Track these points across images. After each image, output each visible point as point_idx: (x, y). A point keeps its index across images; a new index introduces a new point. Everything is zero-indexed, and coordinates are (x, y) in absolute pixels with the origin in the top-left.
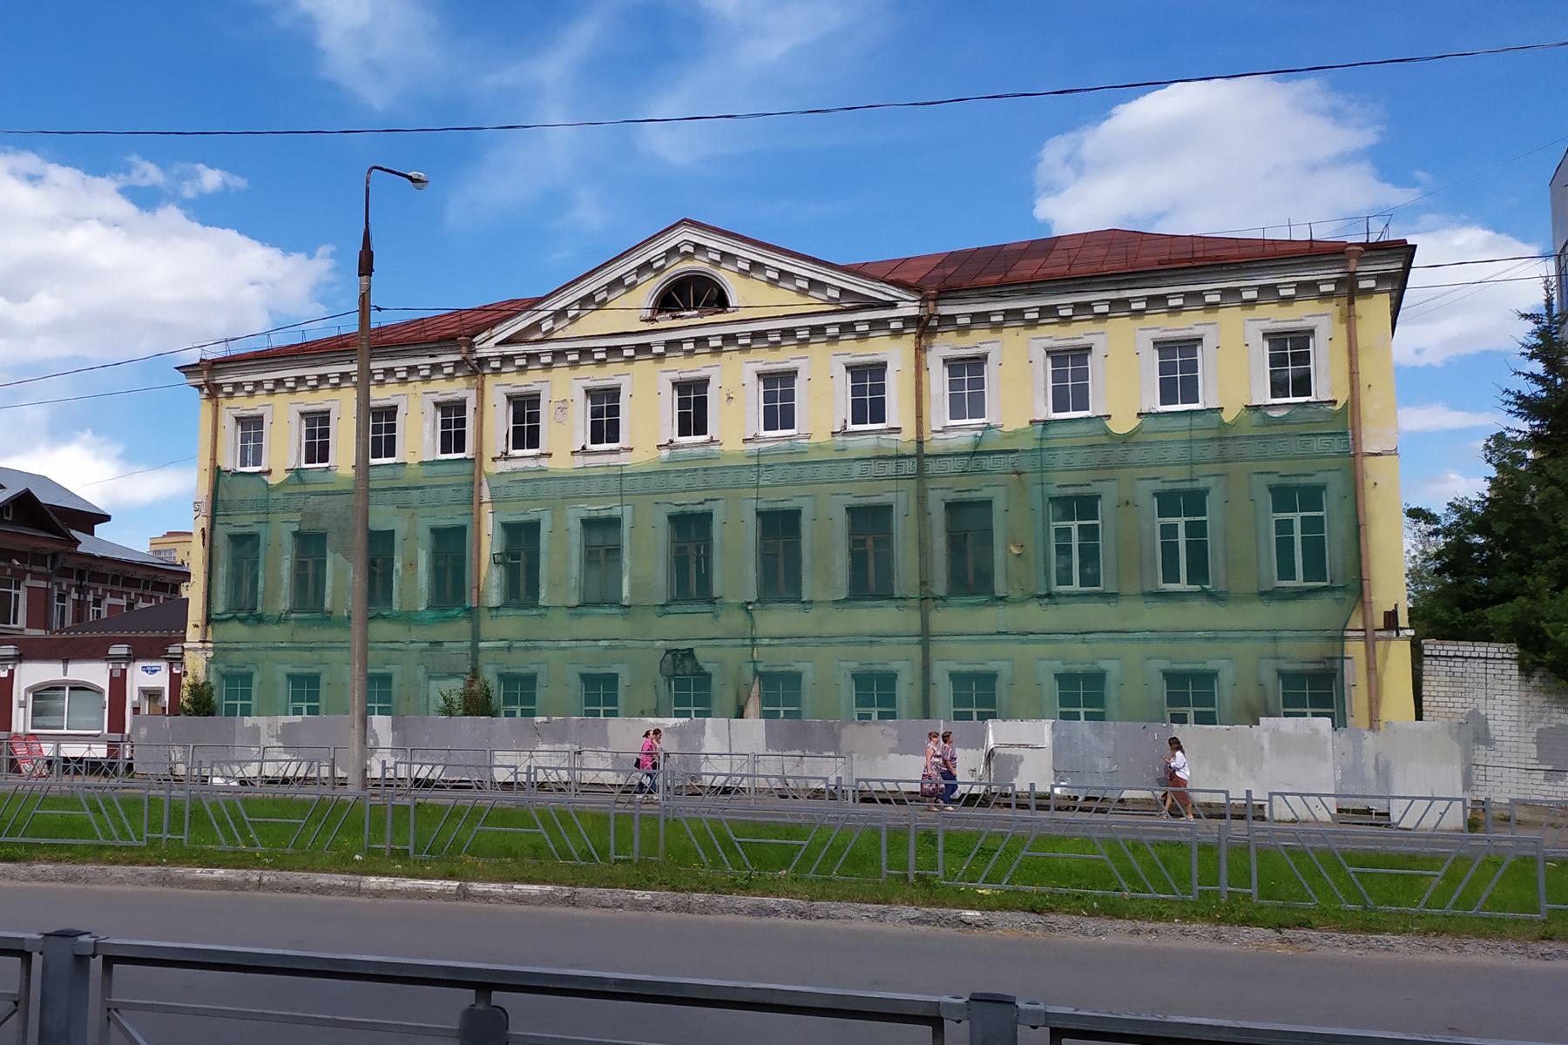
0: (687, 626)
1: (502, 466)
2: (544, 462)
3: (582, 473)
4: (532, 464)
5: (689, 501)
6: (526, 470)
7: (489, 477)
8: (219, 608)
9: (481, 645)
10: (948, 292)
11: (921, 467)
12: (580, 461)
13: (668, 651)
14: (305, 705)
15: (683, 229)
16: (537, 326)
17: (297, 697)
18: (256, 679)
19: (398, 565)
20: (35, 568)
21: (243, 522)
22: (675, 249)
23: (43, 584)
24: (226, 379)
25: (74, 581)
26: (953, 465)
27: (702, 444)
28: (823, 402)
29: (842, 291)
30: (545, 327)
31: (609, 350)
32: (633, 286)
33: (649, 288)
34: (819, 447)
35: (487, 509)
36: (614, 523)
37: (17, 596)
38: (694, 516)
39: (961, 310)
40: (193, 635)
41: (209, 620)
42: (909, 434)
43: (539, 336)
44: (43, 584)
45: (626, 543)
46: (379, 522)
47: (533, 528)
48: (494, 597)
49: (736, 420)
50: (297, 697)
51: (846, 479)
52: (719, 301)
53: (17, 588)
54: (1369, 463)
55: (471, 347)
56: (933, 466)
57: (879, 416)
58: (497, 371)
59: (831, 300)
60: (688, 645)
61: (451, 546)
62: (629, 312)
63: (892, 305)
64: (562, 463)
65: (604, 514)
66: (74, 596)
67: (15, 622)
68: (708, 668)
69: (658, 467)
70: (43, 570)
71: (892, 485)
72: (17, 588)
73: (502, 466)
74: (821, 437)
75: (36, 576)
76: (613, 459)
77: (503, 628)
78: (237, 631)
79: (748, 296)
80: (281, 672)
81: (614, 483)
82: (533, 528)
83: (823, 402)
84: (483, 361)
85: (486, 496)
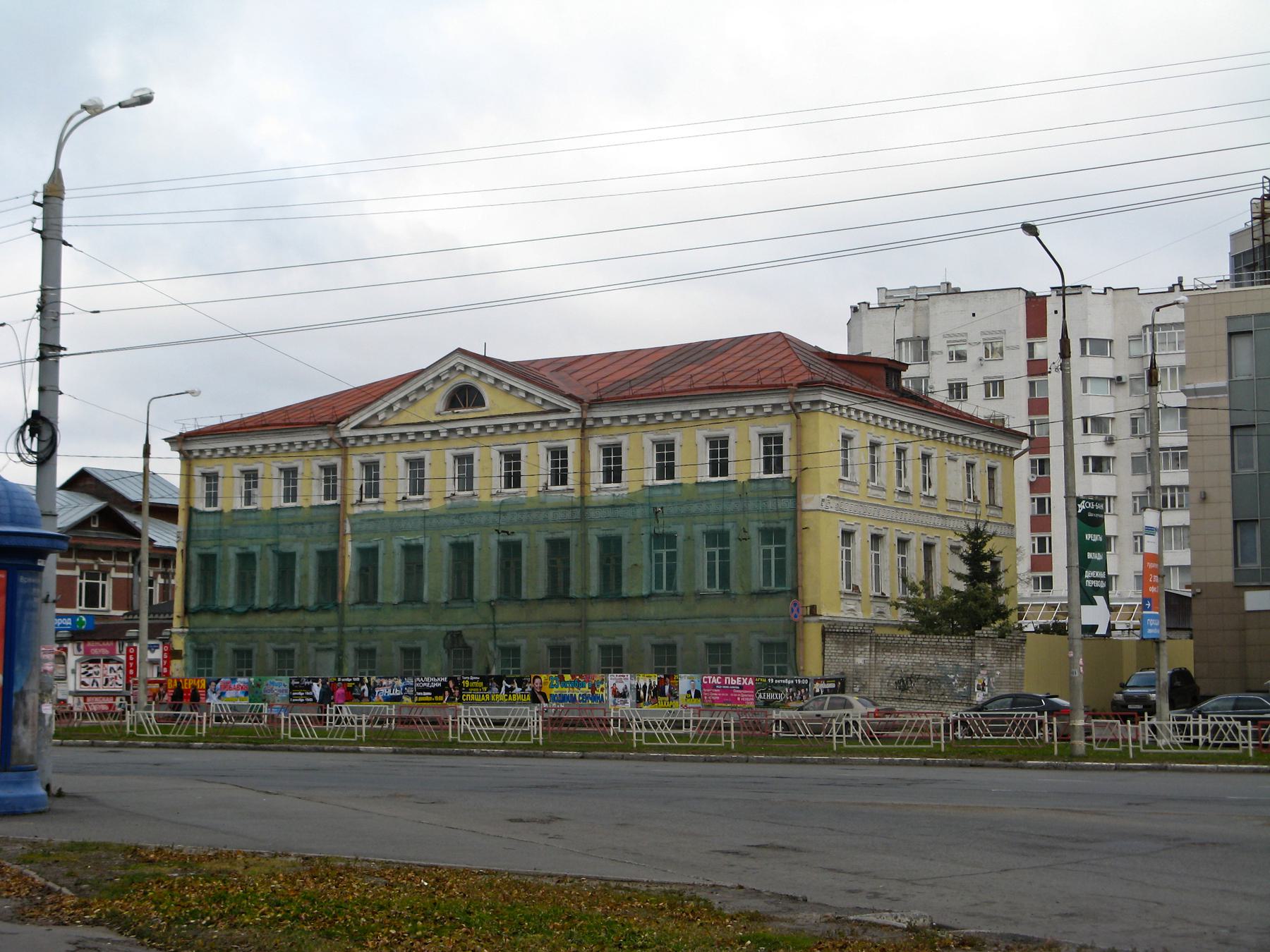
0: (460, 618)
1: (357, 510)
2: (381, 508)
3: (403, 515)
4: (374, 509)
5: (461, 535)
6: (370, 513)
7: (349, 516)
8: (194, 604)
9: (346, 629)
10: (594, 404)
11: (583, 514)
12: (401, 507)
13: (448, 633)
14: (719, 667)
15: (456, 355)
16: (376, 416)
17: (713, 660)
18: (215, 652)
19: (298, 575)
20: (118, 563)
21: (209, 546)
22: (453, 368)
23: (125, 575)
24: (195, 446)
25: (160, 568)
26: (602, 513)
27: (468, 497)
28: (536, 466)
29: (544, 400)
30: (381, 417)
31: (417, 434)
32: (431, 391)
33: (442, 392)
34: (531, 500)
35: (349, 538)
36: (419, 548)
37: (104, 586)
38: (463, 544)
39: (605, 413)
40: (176, 623)
41: (187, 611)
42: (576, 495)
43: (376, 423)
44: (125, 575)
45: (426, 562)
46: (284, 547)
47: (374, 551)
48: (351, 597)
49: (488, 481)
50: (240, 665)
51: (546, 521)
52: (480, 402)
53: (104, 579)
54: (807, 516)
55: (336, 429)
56: (592, 514)
57: (564, 482)
58: (353, 446)
59: (538, 405)
60: (459, 628)
61: (329, 562)
62: (432, 406)
63: (567, 411)
64: (390, 508)
65: (413, 542)
66: (161, 580)
67: (103, 605)
68: (470, 643)
69: (444, 512)
70: (125, 564)
71: (568, 525)
72: (104, 579)
73: (357, 510)
74: (532, 494)
75: (119, 569)
76: (420, 506)
77: (358, 616)
78: (205, 620)
79: (495, 402)
80: (229, 647)
81: (420, 522)
82: (374, 551)
83: (536, 466)
84: (345, 439)
85: (348, 530)
